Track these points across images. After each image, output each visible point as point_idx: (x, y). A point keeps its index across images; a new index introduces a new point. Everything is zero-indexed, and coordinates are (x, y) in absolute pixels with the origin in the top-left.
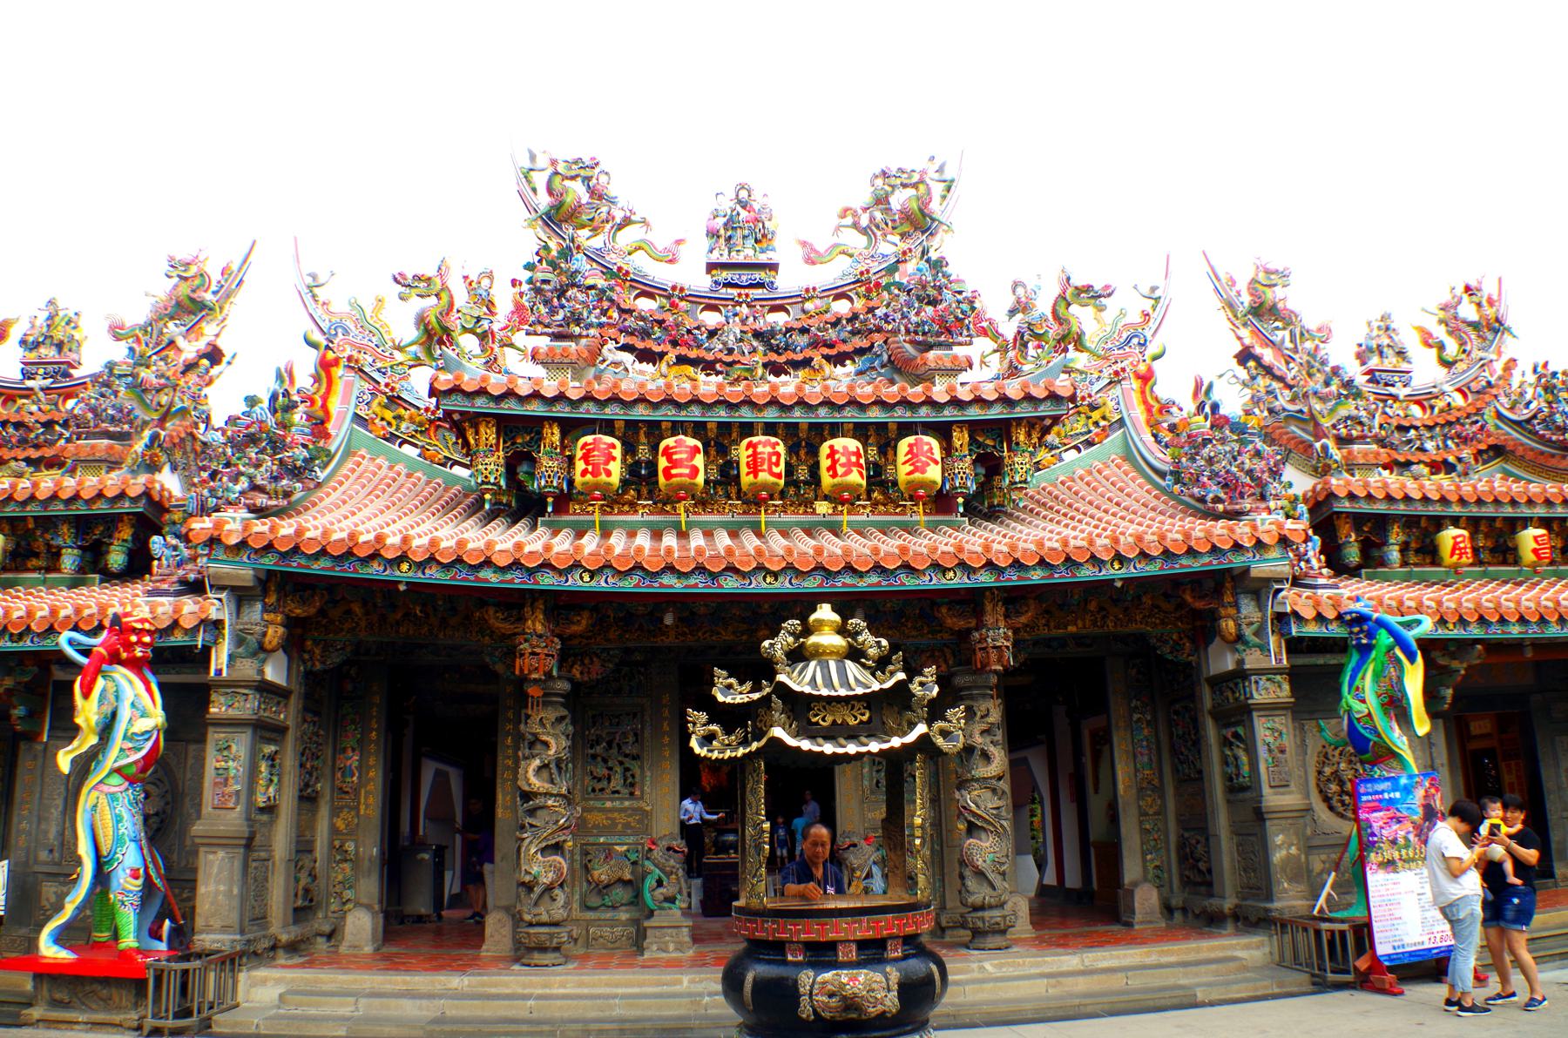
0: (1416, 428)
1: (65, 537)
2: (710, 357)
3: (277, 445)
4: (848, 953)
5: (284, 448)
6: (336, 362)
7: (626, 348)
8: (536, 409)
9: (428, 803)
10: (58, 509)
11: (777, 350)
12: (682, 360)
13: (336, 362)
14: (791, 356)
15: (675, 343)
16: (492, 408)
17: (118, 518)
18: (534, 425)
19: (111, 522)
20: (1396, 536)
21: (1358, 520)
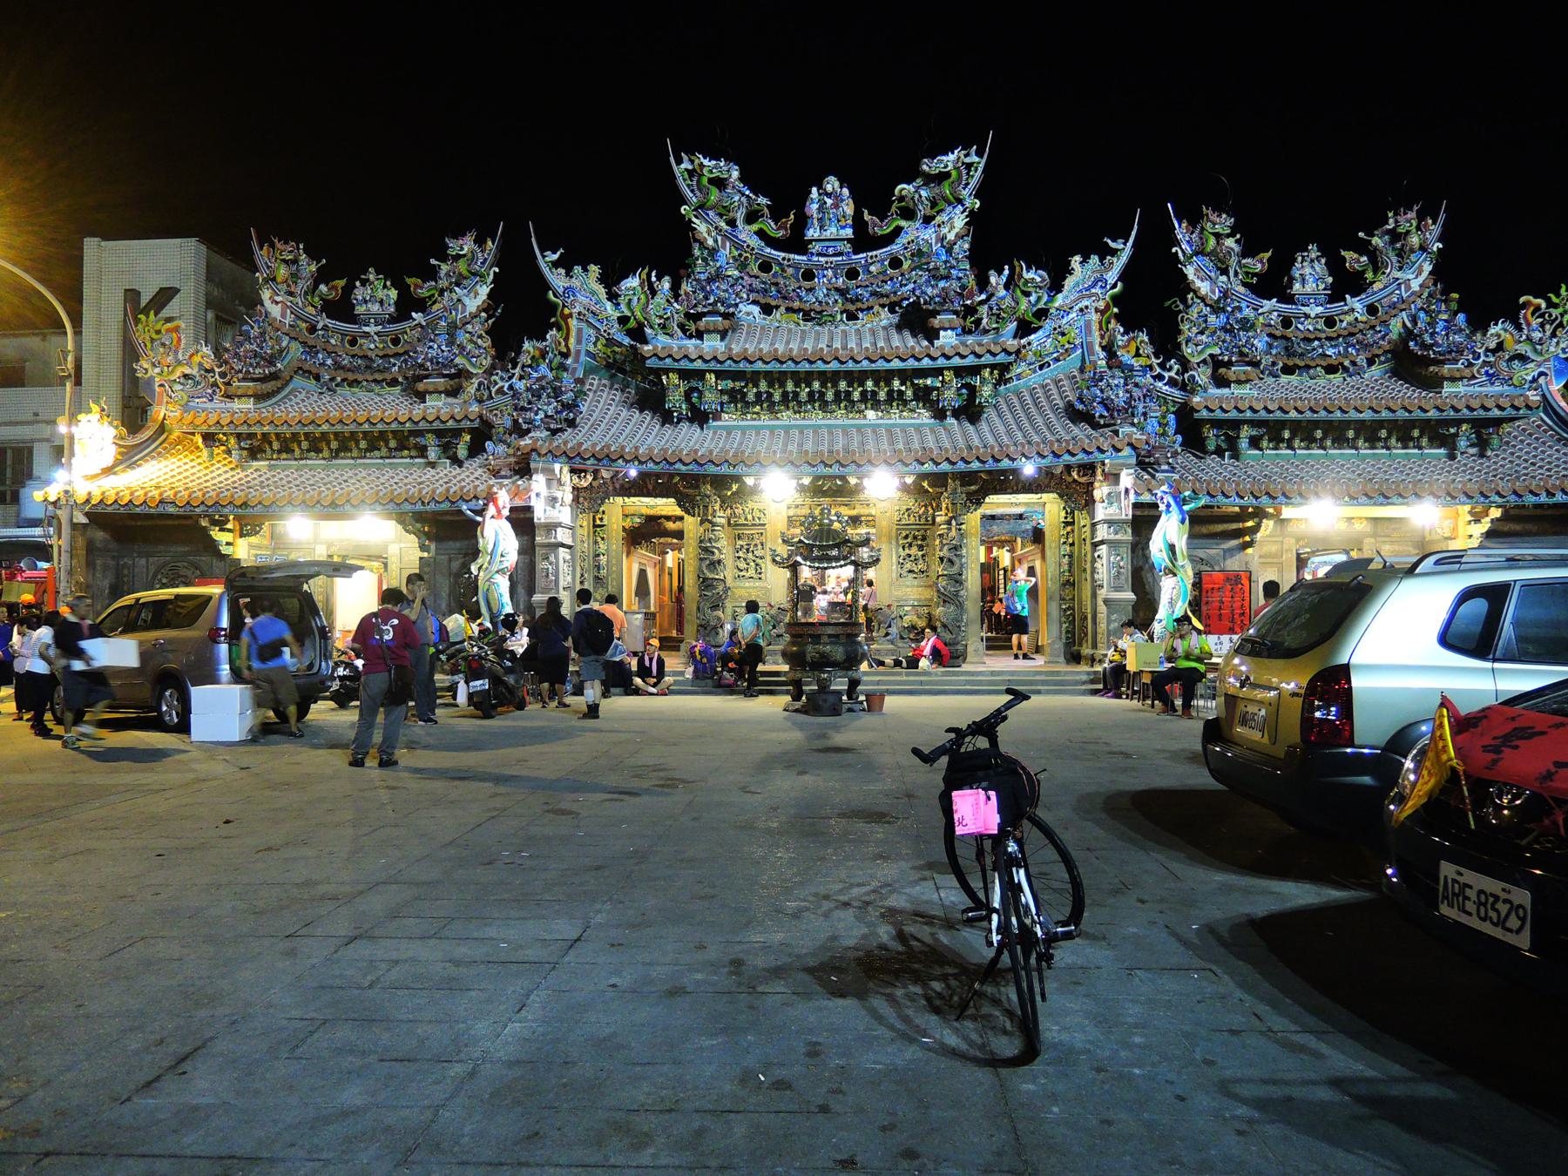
0: (1319, 339)
1: (430, 440)
2: (807, 307)
3: (557, 393)
4: (825, 639)
5: (562, 393)
6: (571, 315)
7: (755, 302)
8: (699, 365)
9: (678, 719)
10: (423, 425)
11: (852, 302)
12: (789, 310)
13: (571, 315)
14: (859, 305)
15: (785, 298)
16: (676, 365)
17: (463, 430)
18: (700, 375)
19: (457, 433)
20: (1246, 432)
21: (1217, 424)
